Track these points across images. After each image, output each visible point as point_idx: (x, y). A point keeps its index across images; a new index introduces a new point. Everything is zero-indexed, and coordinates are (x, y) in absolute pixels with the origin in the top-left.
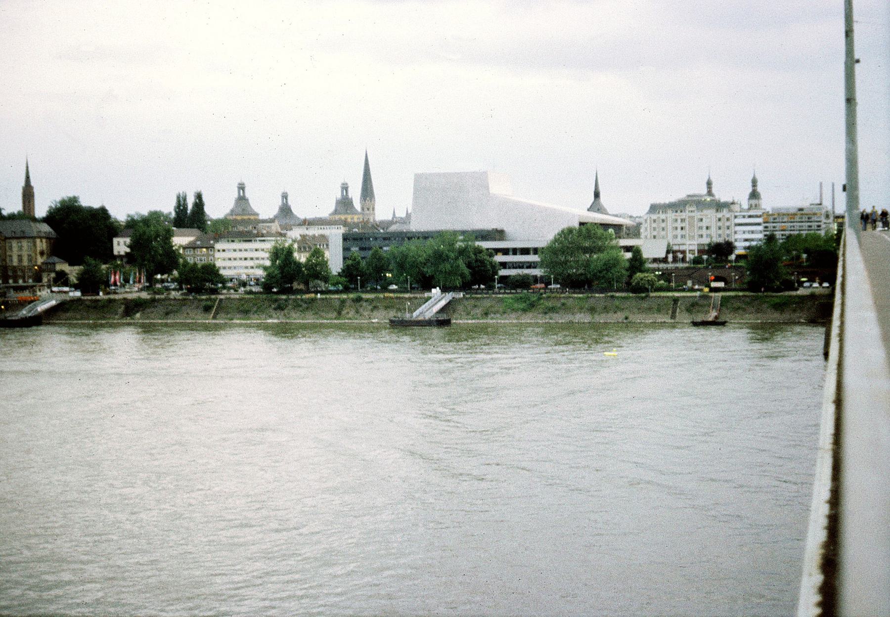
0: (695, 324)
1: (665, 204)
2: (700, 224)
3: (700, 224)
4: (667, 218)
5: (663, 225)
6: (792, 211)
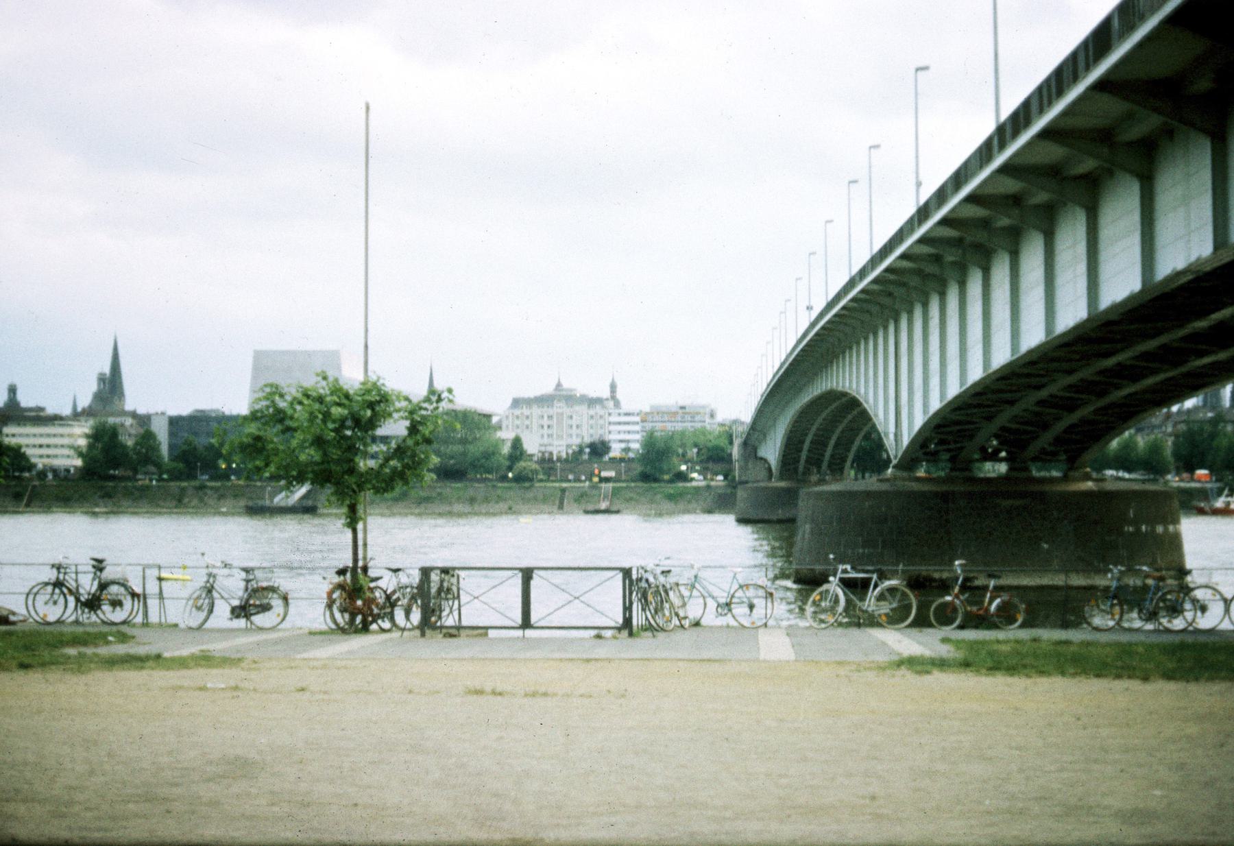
0: (587, 512)
1: (529, 398)
2: (570, 422)
3: (570, 422)
4: (531, 413)
5: (527, 422)
6: (673, 410)
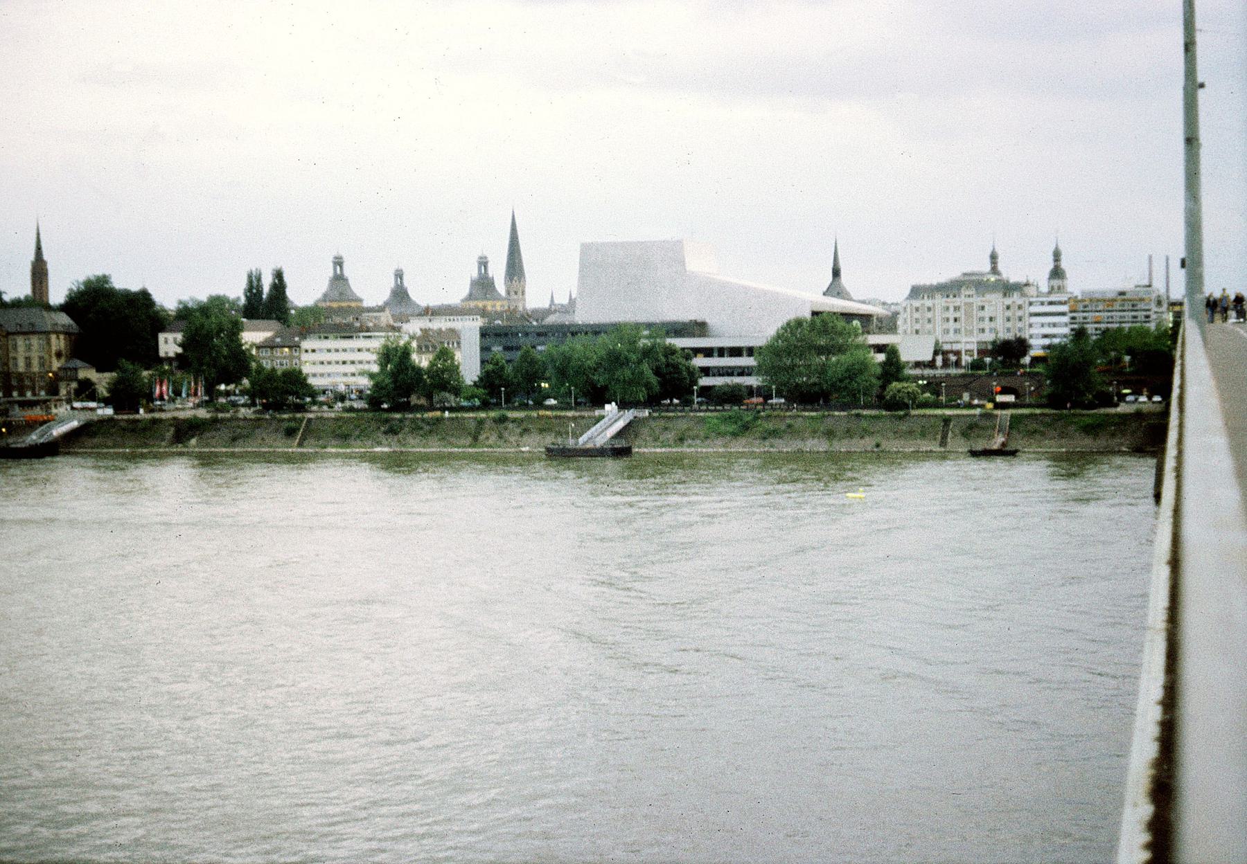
0: (974, 454)
1: (931, 285)
2: (981, 314)
3: (981, 314)
4: (934, 305)
5: (929, 315)
6: (1110, 296)
